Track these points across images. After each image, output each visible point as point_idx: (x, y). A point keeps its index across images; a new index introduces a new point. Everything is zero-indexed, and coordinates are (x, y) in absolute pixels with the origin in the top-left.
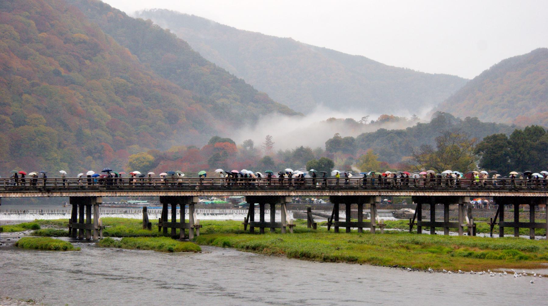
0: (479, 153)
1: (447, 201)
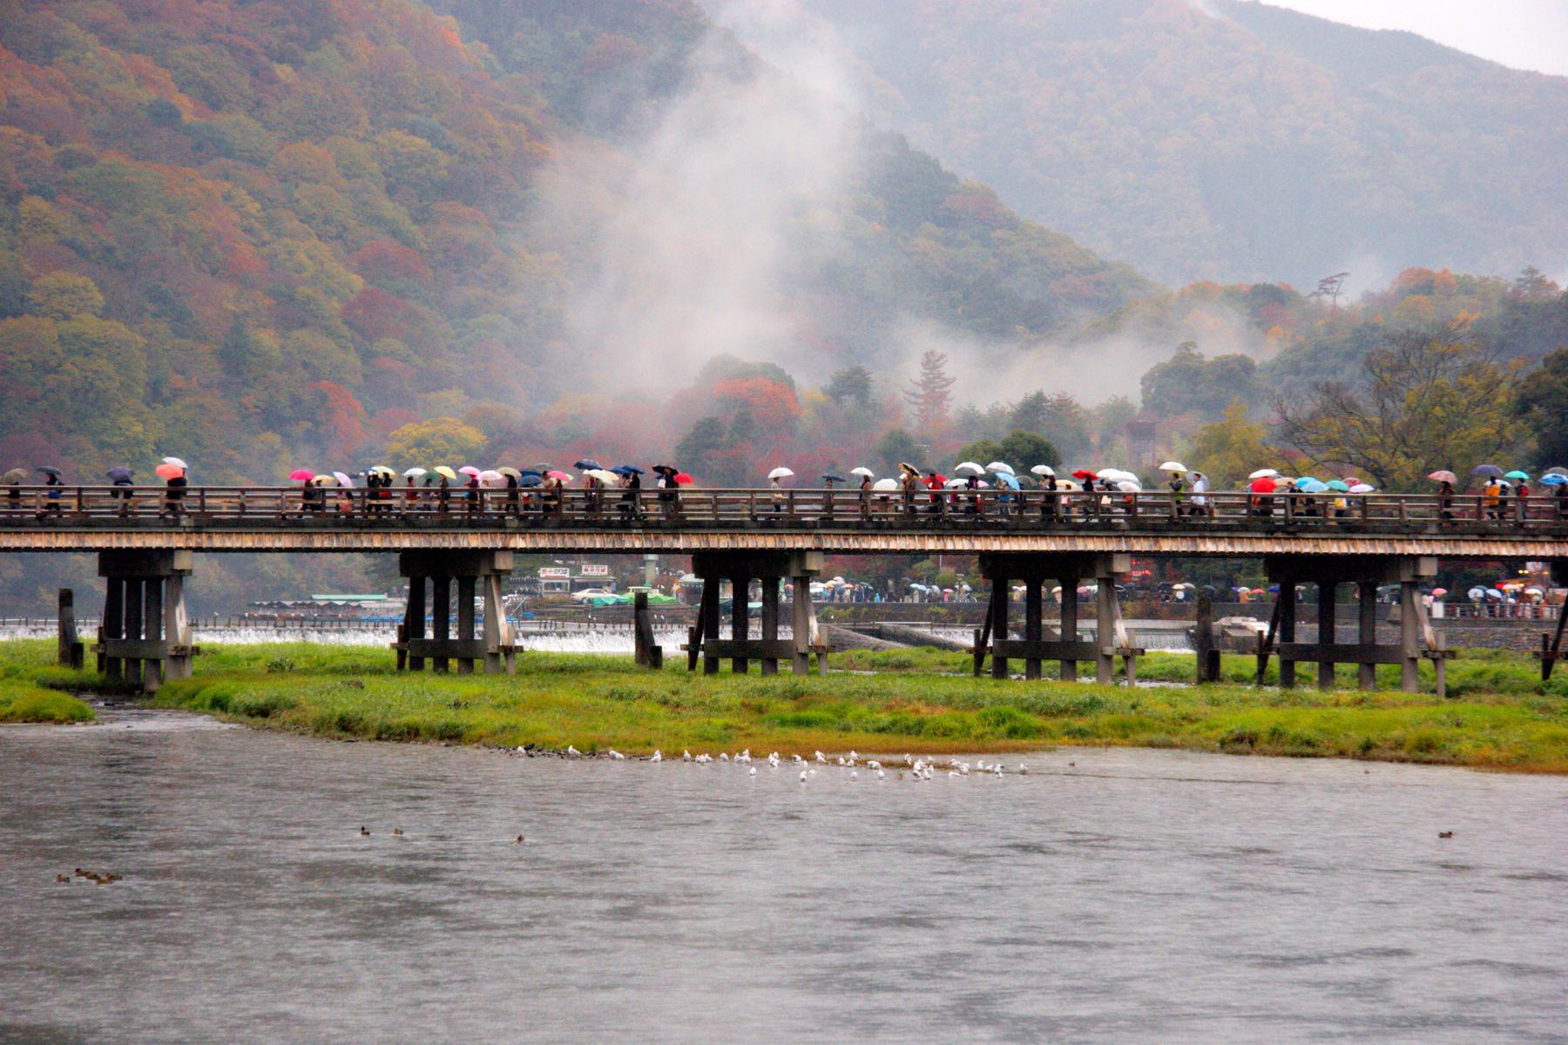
0: (1528, 415)
1: (1071, 568)
